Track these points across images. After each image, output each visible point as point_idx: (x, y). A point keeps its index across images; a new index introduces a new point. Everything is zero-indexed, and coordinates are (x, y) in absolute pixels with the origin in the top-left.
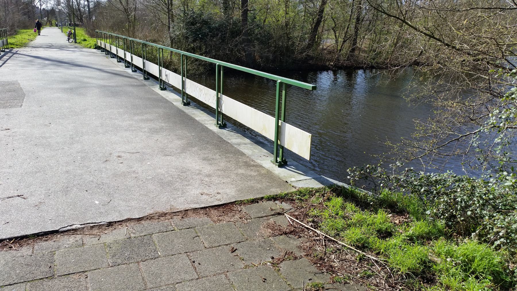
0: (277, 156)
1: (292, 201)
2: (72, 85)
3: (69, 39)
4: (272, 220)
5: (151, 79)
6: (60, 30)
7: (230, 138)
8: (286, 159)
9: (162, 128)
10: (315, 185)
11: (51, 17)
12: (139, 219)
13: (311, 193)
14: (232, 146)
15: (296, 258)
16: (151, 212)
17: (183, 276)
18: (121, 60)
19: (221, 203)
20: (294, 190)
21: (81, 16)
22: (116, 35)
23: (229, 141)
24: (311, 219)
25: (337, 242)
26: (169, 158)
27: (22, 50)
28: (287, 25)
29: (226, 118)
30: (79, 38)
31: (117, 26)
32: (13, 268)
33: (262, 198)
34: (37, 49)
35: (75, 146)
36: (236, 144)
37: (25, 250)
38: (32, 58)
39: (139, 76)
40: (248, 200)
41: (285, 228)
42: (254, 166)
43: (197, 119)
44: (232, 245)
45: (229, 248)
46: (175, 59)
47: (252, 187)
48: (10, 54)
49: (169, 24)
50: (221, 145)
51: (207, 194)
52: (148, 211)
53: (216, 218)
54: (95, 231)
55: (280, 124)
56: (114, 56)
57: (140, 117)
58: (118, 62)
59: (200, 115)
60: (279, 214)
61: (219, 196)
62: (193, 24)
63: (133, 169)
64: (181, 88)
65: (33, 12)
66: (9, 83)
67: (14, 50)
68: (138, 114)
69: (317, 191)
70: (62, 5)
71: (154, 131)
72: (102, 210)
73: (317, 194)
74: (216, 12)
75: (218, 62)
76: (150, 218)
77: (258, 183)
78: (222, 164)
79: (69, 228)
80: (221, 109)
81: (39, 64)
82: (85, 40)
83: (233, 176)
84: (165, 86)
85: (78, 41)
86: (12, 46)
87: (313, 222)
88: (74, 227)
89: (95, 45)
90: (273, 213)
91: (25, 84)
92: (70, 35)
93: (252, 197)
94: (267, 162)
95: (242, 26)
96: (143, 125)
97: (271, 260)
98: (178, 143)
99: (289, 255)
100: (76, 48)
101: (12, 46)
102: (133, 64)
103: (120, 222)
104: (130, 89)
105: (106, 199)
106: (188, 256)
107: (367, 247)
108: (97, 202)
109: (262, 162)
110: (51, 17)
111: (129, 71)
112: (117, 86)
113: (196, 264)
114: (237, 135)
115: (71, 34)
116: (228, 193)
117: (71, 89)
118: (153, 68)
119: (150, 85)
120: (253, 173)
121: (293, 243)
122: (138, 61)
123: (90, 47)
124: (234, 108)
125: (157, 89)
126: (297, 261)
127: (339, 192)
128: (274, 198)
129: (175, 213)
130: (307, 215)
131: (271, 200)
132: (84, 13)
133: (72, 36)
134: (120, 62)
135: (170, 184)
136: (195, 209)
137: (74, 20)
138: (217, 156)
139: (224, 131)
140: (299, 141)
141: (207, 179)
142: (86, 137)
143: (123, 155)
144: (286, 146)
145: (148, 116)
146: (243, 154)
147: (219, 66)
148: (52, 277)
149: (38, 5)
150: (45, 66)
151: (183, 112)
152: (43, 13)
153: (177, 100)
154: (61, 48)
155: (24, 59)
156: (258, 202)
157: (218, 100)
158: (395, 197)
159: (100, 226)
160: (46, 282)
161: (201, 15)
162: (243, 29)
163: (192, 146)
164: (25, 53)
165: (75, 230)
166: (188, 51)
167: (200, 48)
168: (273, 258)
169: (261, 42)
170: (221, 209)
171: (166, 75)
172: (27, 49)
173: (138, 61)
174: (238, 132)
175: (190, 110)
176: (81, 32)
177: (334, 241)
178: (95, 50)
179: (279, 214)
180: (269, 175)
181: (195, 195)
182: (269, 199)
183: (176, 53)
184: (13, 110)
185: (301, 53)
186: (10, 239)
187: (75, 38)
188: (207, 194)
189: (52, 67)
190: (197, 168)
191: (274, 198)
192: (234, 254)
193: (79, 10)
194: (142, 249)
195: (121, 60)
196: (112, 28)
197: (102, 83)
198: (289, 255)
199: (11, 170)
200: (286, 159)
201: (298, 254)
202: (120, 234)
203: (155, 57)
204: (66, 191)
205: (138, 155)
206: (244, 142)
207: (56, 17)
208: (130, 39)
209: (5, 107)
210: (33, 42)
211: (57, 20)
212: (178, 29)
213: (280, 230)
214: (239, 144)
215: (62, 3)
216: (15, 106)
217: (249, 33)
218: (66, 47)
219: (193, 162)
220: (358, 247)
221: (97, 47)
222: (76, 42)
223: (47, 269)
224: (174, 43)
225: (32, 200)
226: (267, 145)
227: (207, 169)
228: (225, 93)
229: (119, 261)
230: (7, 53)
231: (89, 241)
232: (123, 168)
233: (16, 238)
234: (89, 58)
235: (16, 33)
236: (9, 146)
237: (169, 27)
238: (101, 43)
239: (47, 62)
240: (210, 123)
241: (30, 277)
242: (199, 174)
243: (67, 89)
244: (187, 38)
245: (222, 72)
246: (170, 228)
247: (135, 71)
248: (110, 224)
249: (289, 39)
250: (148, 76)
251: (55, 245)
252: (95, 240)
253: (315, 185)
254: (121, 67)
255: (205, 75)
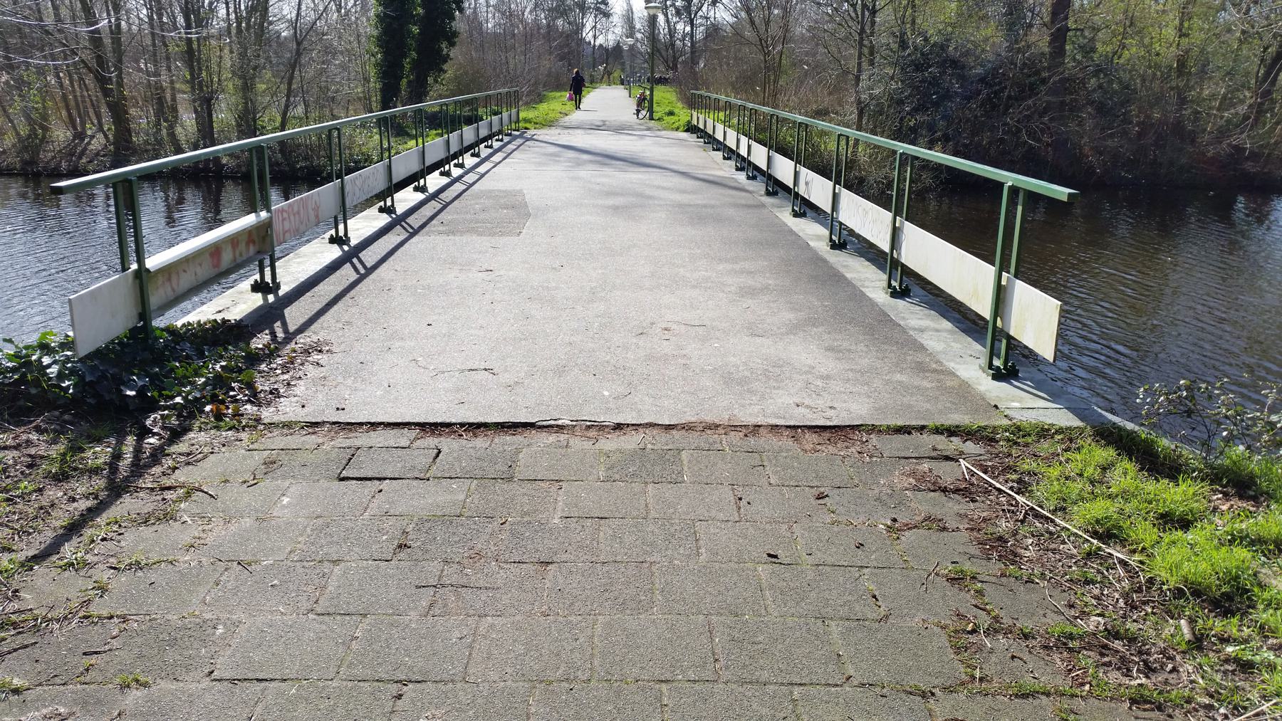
0: (993, 353)
1: (992, 441)
2: (619, 201)
3: (638, 111)
4: (926, 466)
5: (781, 193)
6: (626, 93)
7: (906, 316)
8: (1012, 363)
9: (765, 289)
10: (1063, 418)
11: (612, 64)
12: (669, 427)
13: (1044, 432)
14: (903, 330)
15: (944, 529)
16: (693, 419)
17: (713, 513)
18: (730, 154)
19: (829, 424)
20: (1006, 422)
21: (675, 59)
22: (740, 102)
23: (902, 323)
24: (1014, 477)
25: (1053, 521)
26: (758, 340)
27: (544, 134)
28: (1182, 63)
29: (907, 272)
30: (659, 111)
31: (744, 84)
32: (459, 459)
33: (922, 429)
34: (571, 131)
35: (595, 305)
36: (915, 329)
37: (480, 442)
38: (558, 149)
39: (759, 186)
40: (888, 427)
41: (948, 480)
42: (935, 371)
43: (848, 276)
44: (822, 490)
45: (815, 492)
46: (863, 156)
47: (910, 406)
48: (519, 141)
49: (859, 71)
50: (880, 328)
51: (807, 407)
52: (689, 417)
53: (809, 447)
54: (592, 433)
55: (1004, 283)
56: (720, 146)
57: (729, 266)
58: (725, 158)
59: (860, 269)
60: (947, 458)
61: (831, 413)
62: (918, 67)
63: (684, 352)
64: (829, 211)
65: (579, 53)
66: (507, 193)
67: (529, 134)
68: (727, 261)
69: (1060, 431)
70: (639, 36)
71: (750, 292)
72: (611, 405)
73: (1058, 437)
74: (987, 38)
75: (1009, 178)
76: (688, 427)
77: (928, 401)
78: (865, 362)
79: (552, 422)
80: (899, 254)
81: (569, 160)
82: (671, 113)
83: (877, 383)
84: (805, 208)
85: (656, 116)
86: (528, 125)
87: (1020, 481)
88: (560, 422)
89: (689, 122)
90: (934, 454)
91: (532, 197)
92: (641, 101)
93: (900, 423)
94: (968, 363)
95: (1049, 69)
96: (730, 281)
97: (889, 523)
98: (788, 316)
99: (935, 524)
100: (649, 129)
101: (528, 125)
102: (750, 163)
103: (636, 426)
104: (731, 212)
105: (622, 390)
106: (733, 490)
107: (1115, 536)
108: (606, 393)
109: (957, 367)
110: (612, 64)
111: (742, 177)
112: (705, 206)
113: (744, 502)
114: (927, 311)
115: (645, 99)
116: (853, 410)
117: (616, 209)
118: (784, 169)
119: (773, 206)
120: (926, 384)
121: (951, 508)
122: (759, 155)
123: (677, 129)
124: (928, 252)
125: (786, 216)
126: (945, 534)
127: (1108, 435)
128: (952, 432)
129: (735, 428)
130: (1009, 469)
131: (942, 433)
132: (682, 53)
133: (645, 104)
134: (729, 158)
135: (743, 382)
136: (774, 428)
137: (665, 69)
138: (861, 347)
139: (900, 303)
140: (1036, 318)
141: (819, 383)
142: (618, 293)
143: (674, 327)
144: (1012, 333)
145: (747, 265)
146: (922, 348)
147: (1014, 191)
148: (510, 479)
149: (589, 37)
150: (579, 164)
151: (825, 261)
152: (597, 56)
153: (819, 238)
154: (619, 129)
155: (543, 150)
156: (909, 433)
157: (896, 233)
158: (1255, 464)
159: (601, 427)
160: (500, 485)
161: (943, 47)
162: (1050, 77)
163: (814, 325)
164: (547, 138)
165: (561, 427)
166: (899, 136)
167: (931, 128)
168: (894, 520)
169: (1101, 109)
170: (827, 435)
171: (807, 183)
172: (553, 131)
173: (759, 155)
174: (931, 306)
175: (841, 259)
176: (668, 95)
177: (1047, 518)
178: (685, 135)
179: (947, 458)
180: (964, 391)
181: (786, 405)
182: (938, 431)
183: (868, 145)
184: (502, 241)
185: (1218, 140)
186: (462, 425)
187: (651, 110)
188: (807, 407)
189: (591, 167)
190: (809, 362)
191: (952, 432)
192: (821, 501)
193: (673, 45)
194: (658, 468)
195: (730, 154)
196: (736, 89)
197: (678, 197)
198: (935, 524)
199: (482, 332)
200: (1012, 363)
201: (951, 524)
202: (630, 441)
203: (817, 151)
204: (561, 371)
205: (700, 330)
206: (937, 326)
207: (623, 64)
208: (766, 109)
209: (493, 234)
210: (567, 118)
211: (623, 70)
212: (878, 83)
213: (934, 484)
214: (922, 330)
215: (639, 31)
216: (509, 234)
217: (1068, 85)
218: (631, 128)
219: (806, 353)
220: (1095, 534)
221: (691, 129)
222: (651, 118)
223: (506, 468)
224: (869, 116)
225: (506, 378)
226: (970, 329)
227: (829, 365)
228: (848, 187)
229: (617, 477)
230: (517, 137)
231: (577, 443)
232: (667, 348)
233: (471, 425)
234: (667, 150)
235: (541, 99)
236: (487, 296)
237: (858, 79)
238: (699, 118)
239: (585, 157)
240: (873, 283)
241: (479, 473)
242: (806, 373)
243: (609, 207)
244: (901, 102)
245: (1020, 208)
246: (718, 446)
247: (754, 178)
248: (618, 427)
249: (1183, 101)
250: (776, 187)
251: (526, 442)
252: (587, 445)
253: (1063, 418)
254: (727, 170)
255: (961, 212)
